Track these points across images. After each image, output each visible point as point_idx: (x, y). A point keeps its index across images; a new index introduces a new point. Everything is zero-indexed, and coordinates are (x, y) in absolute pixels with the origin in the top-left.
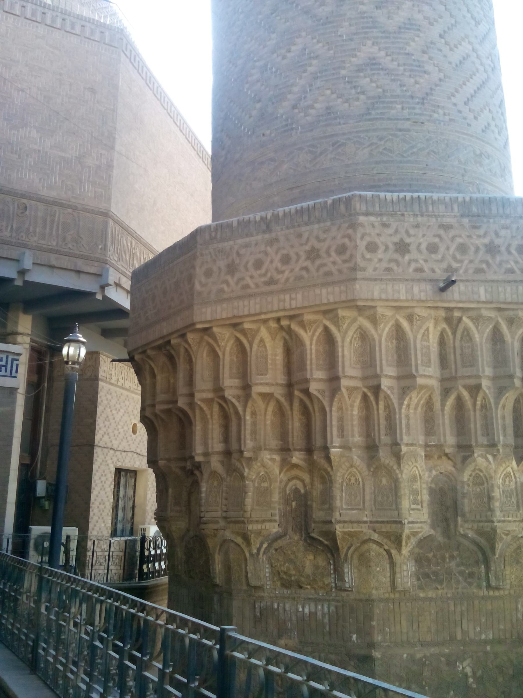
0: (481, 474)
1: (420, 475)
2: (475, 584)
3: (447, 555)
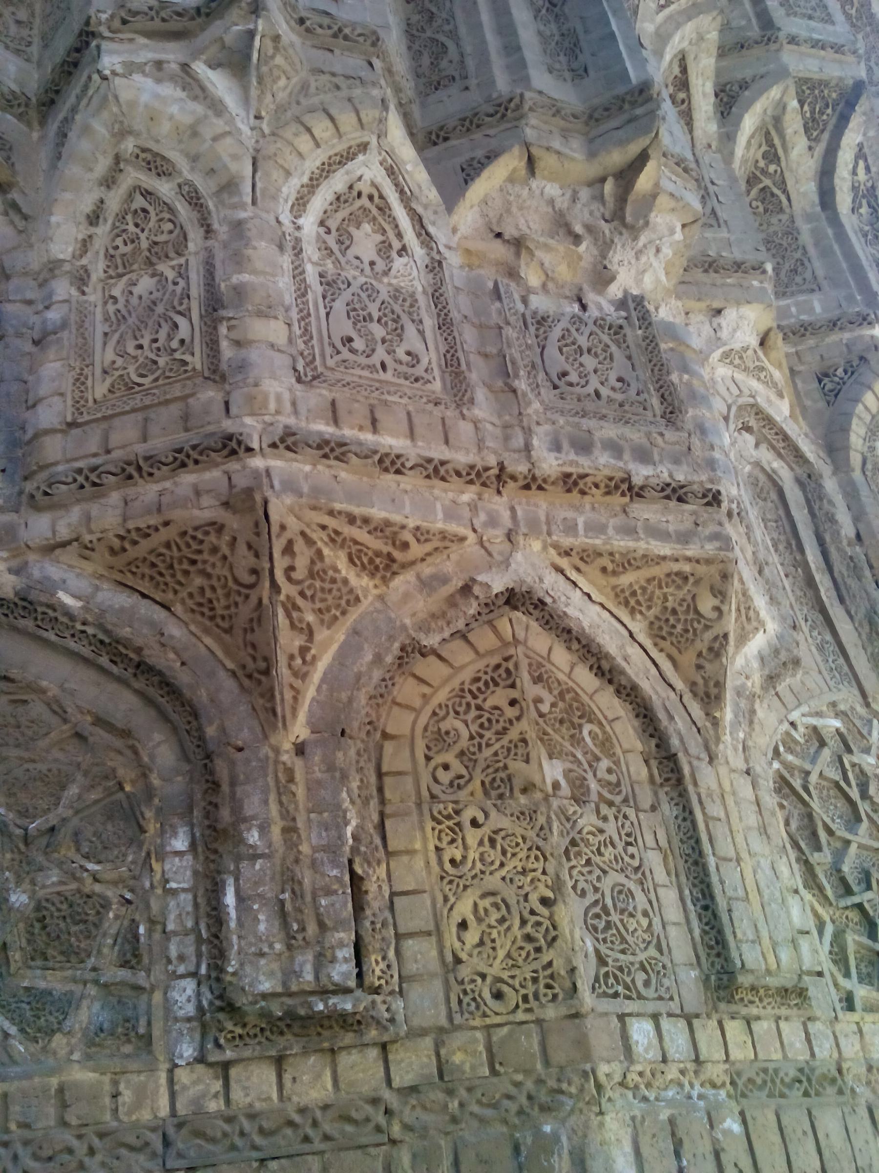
0: (165, 189)
2: (89, 1012)
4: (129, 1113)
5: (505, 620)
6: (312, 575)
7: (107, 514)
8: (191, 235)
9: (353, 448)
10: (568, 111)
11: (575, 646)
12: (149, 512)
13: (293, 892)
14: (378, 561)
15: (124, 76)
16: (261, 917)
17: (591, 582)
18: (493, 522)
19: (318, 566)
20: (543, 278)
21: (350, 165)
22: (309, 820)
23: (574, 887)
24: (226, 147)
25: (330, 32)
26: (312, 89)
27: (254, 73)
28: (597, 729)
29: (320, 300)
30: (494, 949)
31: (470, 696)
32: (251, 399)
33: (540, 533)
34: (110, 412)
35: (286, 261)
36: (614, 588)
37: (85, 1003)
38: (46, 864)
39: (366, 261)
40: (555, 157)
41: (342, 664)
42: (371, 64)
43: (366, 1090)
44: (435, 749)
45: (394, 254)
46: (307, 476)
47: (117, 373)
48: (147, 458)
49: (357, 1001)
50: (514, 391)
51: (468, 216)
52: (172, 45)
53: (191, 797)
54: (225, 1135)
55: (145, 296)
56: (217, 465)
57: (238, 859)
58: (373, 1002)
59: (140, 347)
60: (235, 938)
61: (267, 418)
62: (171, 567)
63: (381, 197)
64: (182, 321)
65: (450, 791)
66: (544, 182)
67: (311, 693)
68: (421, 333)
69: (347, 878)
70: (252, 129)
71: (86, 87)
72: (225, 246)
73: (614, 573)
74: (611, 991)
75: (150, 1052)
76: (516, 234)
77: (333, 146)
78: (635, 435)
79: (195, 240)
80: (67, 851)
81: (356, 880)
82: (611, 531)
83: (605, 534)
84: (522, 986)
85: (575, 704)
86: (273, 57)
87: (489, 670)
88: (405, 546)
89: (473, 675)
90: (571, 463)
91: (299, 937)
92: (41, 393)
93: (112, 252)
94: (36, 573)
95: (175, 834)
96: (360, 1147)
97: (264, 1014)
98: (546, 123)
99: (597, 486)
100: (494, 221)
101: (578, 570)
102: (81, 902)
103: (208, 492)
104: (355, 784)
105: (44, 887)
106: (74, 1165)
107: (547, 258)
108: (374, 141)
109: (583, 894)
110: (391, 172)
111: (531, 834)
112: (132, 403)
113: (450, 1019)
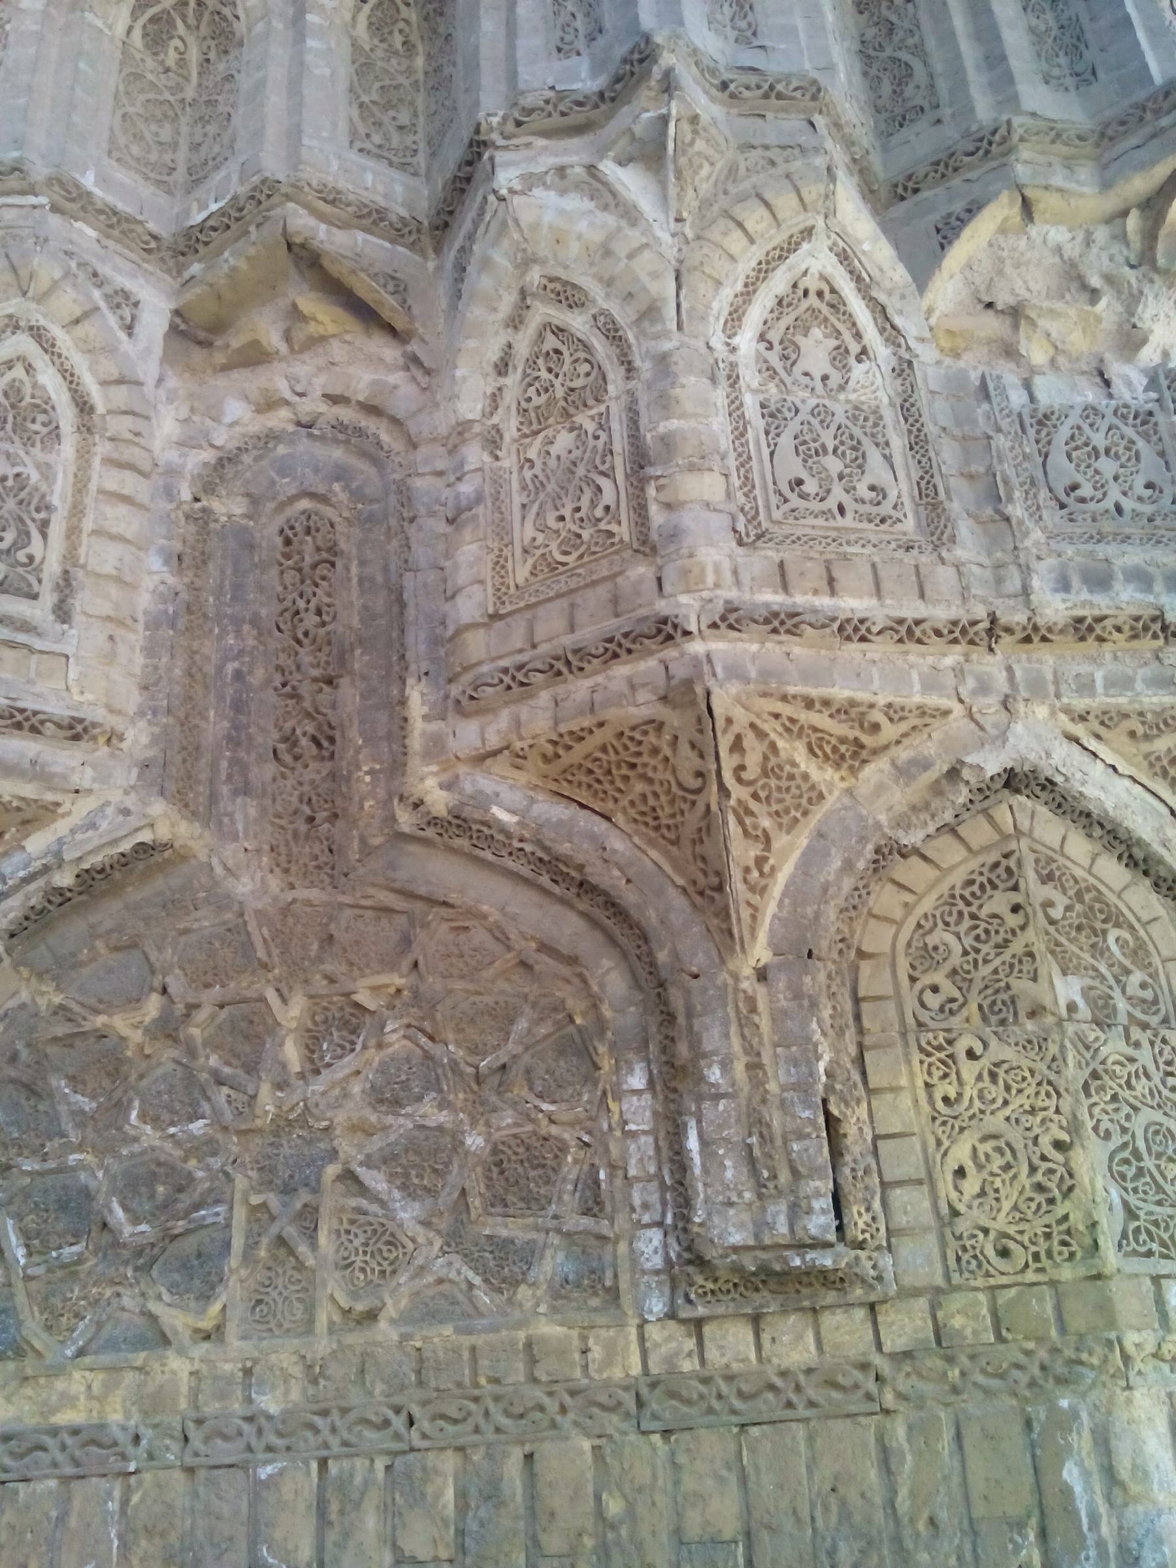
0: (578, 323)
1: (84, 407)
2: (553, 1263)
3: (292, 1013)
4: (599, 1371)
5: (1005, 806)
6: (765, 773)
7: (537, 716)
8: (610, 376)
10: (1072, 133)
11: (1097, 832)
12: (582, 713)
13: (761, 1136)
14: (843, 749)
16: (728, 1163)
17: (1115, 750)
18: (984, 688)
19: (773, 761)
20: (1051, 351)
22: (776, 1055)
23: (1095, 1129)
24: (645, 263)
25: (760, 92)
26: (742, 171)
28: (1126, 935)
29: (763, 437)
31: (962, 903)
34: (533, 600)
35: (720, 396)
36: (1146, 756)
37: (549, 1253)
38: (499, 1104)
39: (818, 377)
40: (1057, 196)
41: (806, 874)
42: (812, 124)
43: (853, 1353)
45: (852, 361)
46: (754, 658)
48: (575, 652)
49: (838, 1256)
51: (948, 288)
52: (575, 142)
53: (645, 1029)
54: (701, 1397)
55: (564, 455)
56: (651, 653)
57: (699, 1099)
58: (857, 1258)
60: (700, 1186)
61: (705, 594)
62: (609, 772)
63: (833, 291)
64: (604, 483)
66: (1047, 227)
67: (771, 909)
68: (888, 458)
69: (821, 1120)
70: (673, 235)
71: (481, 212)
72: (649, 386)
73: (1147, 738)
74: (1143, 1249)
75: (618, 1306)
76: (1012, 301)
77: (771, 238)
80: (520, 1091)
81: (831, 1122)
82: (1139, 686)
83: (1132, 689)
87: (985, 870)
88: (876, 727)
89: (966, 877)
90: (1084, 604)
91: (771, 1185)
92: (460, 582)
93: (524, 405)
94: (468, 788)
95: (631, 1071)
96: (848, 1416)
97: (737, 1269)
98: (1043, 153)
99: (1119, 630)
101: (1098, 737)
103: (644, 685)
104: (826, 1013)
105: (499, 1129)
106: (545, 1423)
107: (1054, 327)
108: (820, 222)
109: (1108, 1135)
110: (844, 257)
111: (1041, 1067)
112: (556, 587)
113: (947, 1277)
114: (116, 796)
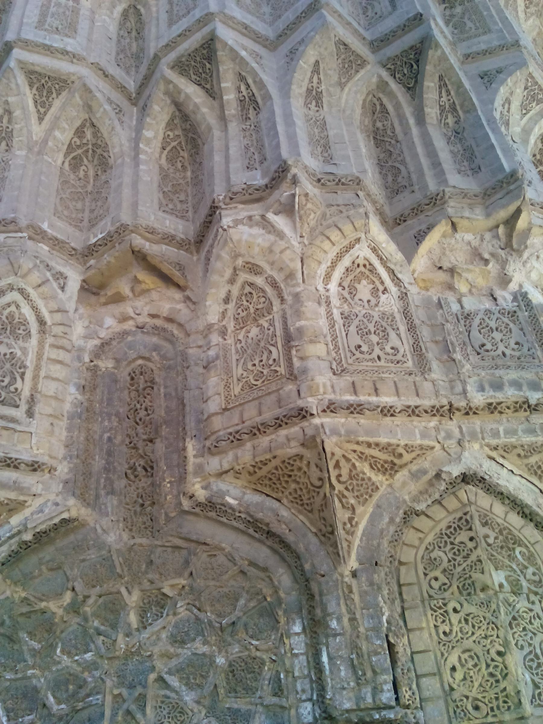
0: (259, 281)
3: (133, 599)
5: (463, 491)
6: (351, 478)
7: (246, 454)
8: (274, 303)
9: (366, 406)
10: (472, 194)
11: (507, 502)
12: (265, 452)
13: (358, 654)
14: (386, 466)
15: (233, 227)
16: (342, 668)
17: (511, 463)
18: (449, 436)
20: (469, 287)
21: (352, 251)
22: (362, 614)
23: (516, 645)
26: (328, 216)
27: (297, 215)
28: (524, 550)
30: (472, 682)
31: (447, 536)
32: (310, 388)
33: (478, 439)
35: (322, 310)
36: (526, 465)
37: (257, 716)
38: (232, 642)
39: (365, 301)
44: (429, 569)
45: (380, 294)
46: (343, 425)
47: (244, 380)
48: (262, 424)
50: (454, 360)
51: (421, 261)
52: (256, 205)
56: (296, 424)
57: (327, 636)
58: (406, 713)
59: (254, 365)
61: (319, 397)
62: (279, 479)
63: (370, 264)
64: (273, 349)
65: (440, 592)
66: (463, 234)
67: (357, 542)
68: (399, 335)
69: (386, 645)
71: (216, 236)
73: (526, 457)
76: (450, 266)
78: (529, 375)
79: (276, 306)
80: (242, 635)
81: (391, 646)
82: (520, 433)
83: (517, 435)
84: (490, 703)
85: (510, 536)
86: (306, 205)
87: (456, 521)
88: (401, 455)
89: (447, 525)
90: (491, 397)
91: (363, 678)
93: (237, 316)
94: (215, 488)
95: (294, 623)
99: (508, 408)
100: (436, 261)
101: (503, 457)
102: (250, 661)
103: (293, 439)
104: (385, 592)
105: (232, 654)
107: (470, 276)
108: (363, 236)
109: (522, 648)
110: (374, 250)
111: (488, 615)
114: (52, 497)
